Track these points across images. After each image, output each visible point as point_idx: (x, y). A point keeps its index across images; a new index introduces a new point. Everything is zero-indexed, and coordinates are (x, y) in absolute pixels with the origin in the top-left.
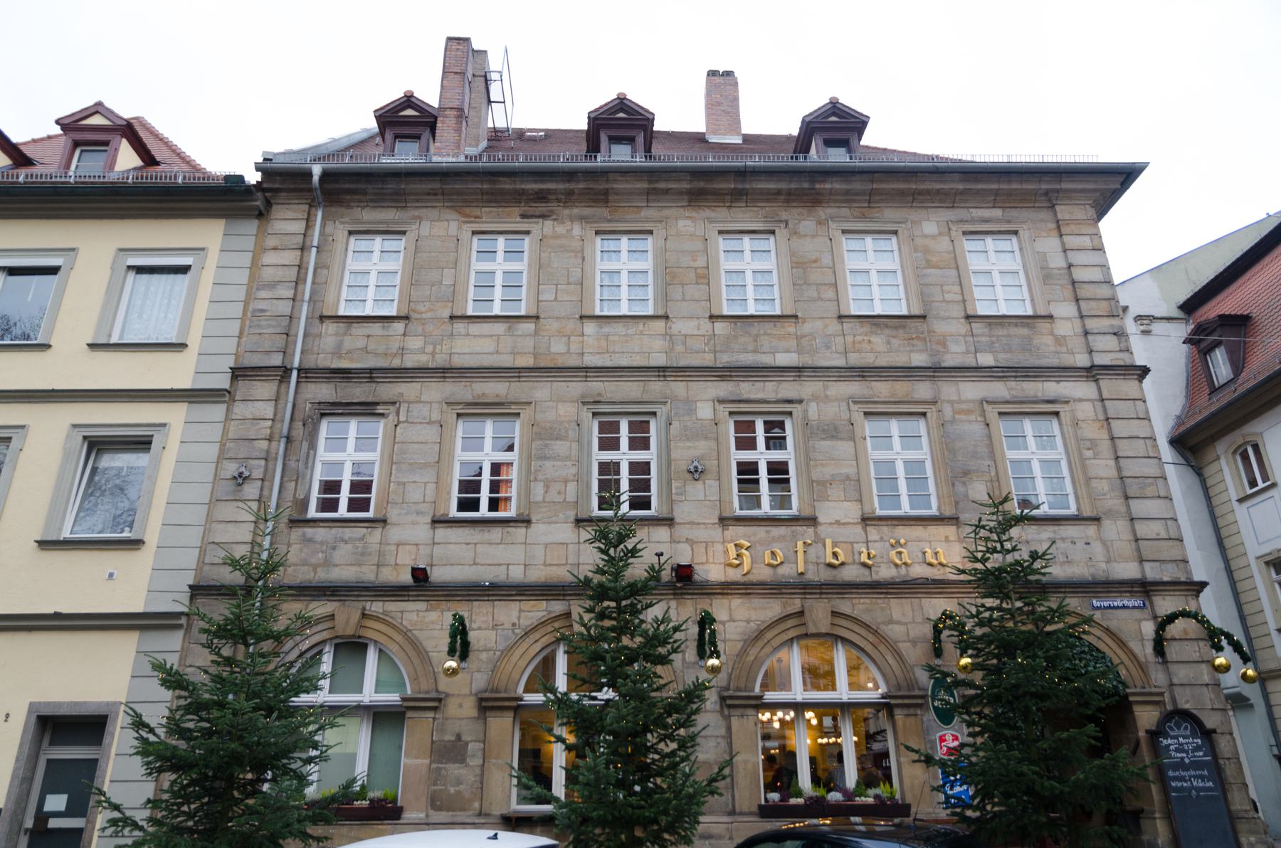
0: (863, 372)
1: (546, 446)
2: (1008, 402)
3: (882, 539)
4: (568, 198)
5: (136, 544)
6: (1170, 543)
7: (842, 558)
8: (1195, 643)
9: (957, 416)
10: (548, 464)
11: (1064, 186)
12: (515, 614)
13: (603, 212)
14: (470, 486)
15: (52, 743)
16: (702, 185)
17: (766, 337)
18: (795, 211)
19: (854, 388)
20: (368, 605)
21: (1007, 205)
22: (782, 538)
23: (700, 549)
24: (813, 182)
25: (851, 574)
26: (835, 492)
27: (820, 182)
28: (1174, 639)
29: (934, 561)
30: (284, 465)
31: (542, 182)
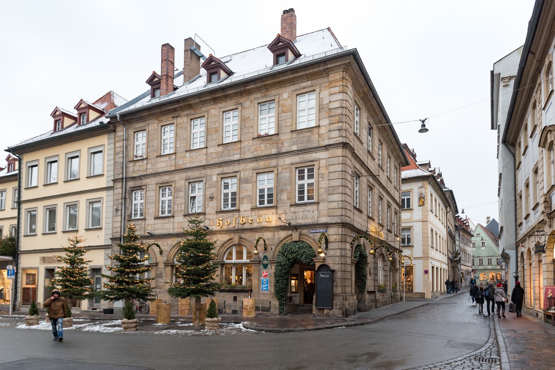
0: (256, 159)
2: (298, 163)
4: (182, 109)
6: (338, 209)
7: (244, 221)
10: (178, 199)
11: (329, 66)
12: (171, 241)
13: (192, 111)
16: (213, 96)
18: (245, 98)
19: (254, 165)
22: (230, 217)
23: (211, 221)
24: (245, 87)
25: (247, 226)
26: (245, 201)
27: (247, 86)
28: (331, 242)
29: (268, 221)
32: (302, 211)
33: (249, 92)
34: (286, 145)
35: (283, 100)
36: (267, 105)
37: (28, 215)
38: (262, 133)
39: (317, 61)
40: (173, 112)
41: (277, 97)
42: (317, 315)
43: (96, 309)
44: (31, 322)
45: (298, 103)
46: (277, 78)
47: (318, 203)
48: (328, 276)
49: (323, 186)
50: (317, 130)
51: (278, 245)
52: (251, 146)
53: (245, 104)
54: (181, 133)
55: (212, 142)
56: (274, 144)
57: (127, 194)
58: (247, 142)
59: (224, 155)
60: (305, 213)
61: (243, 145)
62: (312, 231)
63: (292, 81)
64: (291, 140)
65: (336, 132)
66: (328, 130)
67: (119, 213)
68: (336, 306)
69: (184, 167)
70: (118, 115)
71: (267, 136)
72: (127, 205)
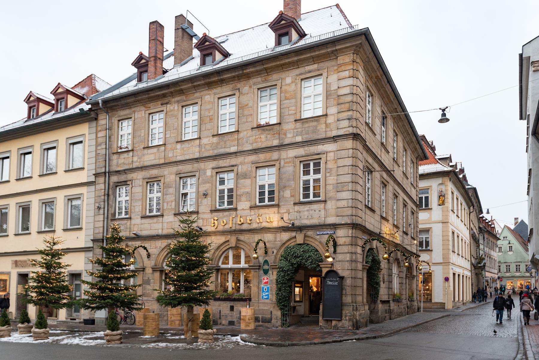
0: (256, 151)
1: (167, 190)
3: (255, 214)
4: (172, 94)
5: (81, 229)
6: (348, 209)
7: (242, 221)
8: (347, 246)
9: (285, 165)
10: (168, 196)
12: (160, 244)
13: (183, 97)
14: (306, 189)
15: (76, 280)
16: (208, 80)
17: (228, 141)
18: (242, 83)
20: (128, 243)
21: (319, 61)
22: (227, 216)
23: (205, 221)
24: (243, 70)
26: (243, 198)
27: (246, 69)
30: (108, 203)
31: (162, 91)
32: (308, 210)
34: (289, 135)
35: (286, 85)
36: (268, 90)
40: (162, 98)
41: (279, 81)
42: (324, 327)
46: (279, 61)
48: (336, 283)
52: (250, 137)
53: (244, 90)
54: (171, 121)
55: (206, 132)
56: (276, 135)
57: (110, 190)
58: (245, 133)
59: (219, 147)
60: (311, 212)
61: (241, 135)
63: (296, 64)
64: (295, 130)
65: (345, 121)
67: (101, 211)
68: (346, 317)
69: (174, 160)
70: (100, 101)
71: (268, 125)
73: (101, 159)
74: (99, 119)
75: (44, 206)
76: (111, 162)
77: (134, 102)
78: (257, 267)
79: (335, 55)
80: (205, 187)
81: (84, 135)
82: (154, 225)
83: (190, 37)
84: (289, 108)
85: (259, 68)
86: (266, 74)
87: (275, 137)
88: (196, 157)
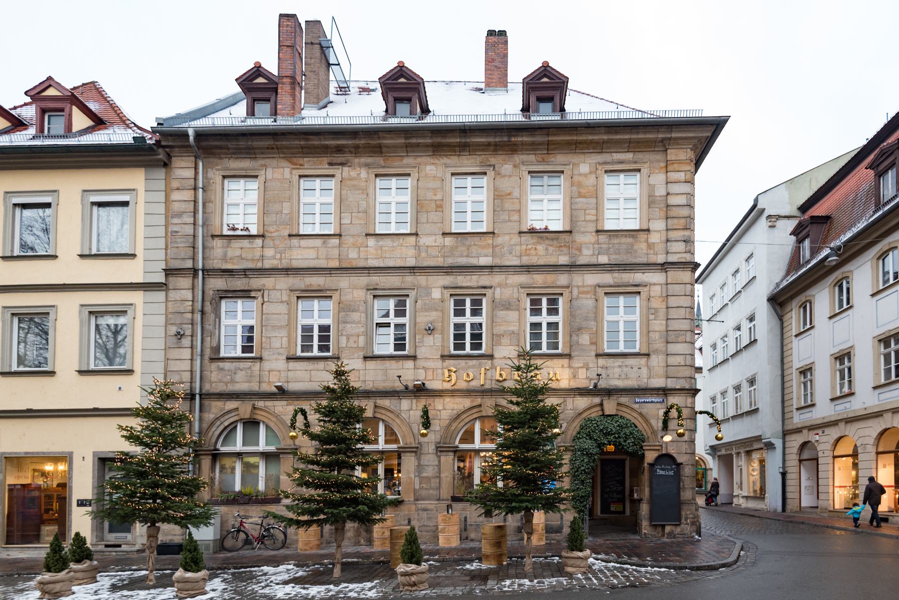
0: (528, 269)
1: (347, 315)
2: (611, 286)
4: (357, 151)
5: (130, 372)
7: (504, 377)
10: (348, 326)
11: (674, 135)
13: (380, 160)
16: (439, 140)
22: (473, 366)
23: (430, 373)
24: (510, 136)
26: (505, 340)
27: (514, 136)
30: (202, 328)
31: (338, 139)
32: (620, 366)
33: (513, 149)
34: (586, 252)
35: (580, 175)
36: (546, 178)
37: (12, 322)
38: (538, 226)
39: (551, 124)
40: (332, 153)
41: (568, 167)
42: (651, 535)
43: (119, 546)
44: (58, 587)
45: (226, 191)
46: (577, 135)
47: (648, 355)
48: (671, 473)
49: (657, 329)
50: (646, 236)
51: (573, 420)
52: (515, 245)
53: (503, 168)
54: (353, 197)
55: (428, 225)
56: (563, 248)
57: (207, 304)
58: (507, 238)
59: (456, 253)
60: (625, 369)
61: (499, 240)
62: (637, 400)
63: (599, 147)
64: (596, 246)
65: (680, 243)
66: (664, 239)
67: (186, 342)
68: (686, 519)
69: (361, 264)
70: (191, 132)
71: (546, 231)
72: (207, 327)
73: (182, 242)
74: (173, 166)
75: (16, 320)
76: (207, 251)
77: (268, 148)
78: (415, 450)
79: (664, 146)
80: (429, 316)
81: (55, 191)
82: (319, 373)
83: (326, 64)
84: (585, 210)
85: (539, 139)
86: (546, 152)
87: (561, 251)
88: (408, 265)
